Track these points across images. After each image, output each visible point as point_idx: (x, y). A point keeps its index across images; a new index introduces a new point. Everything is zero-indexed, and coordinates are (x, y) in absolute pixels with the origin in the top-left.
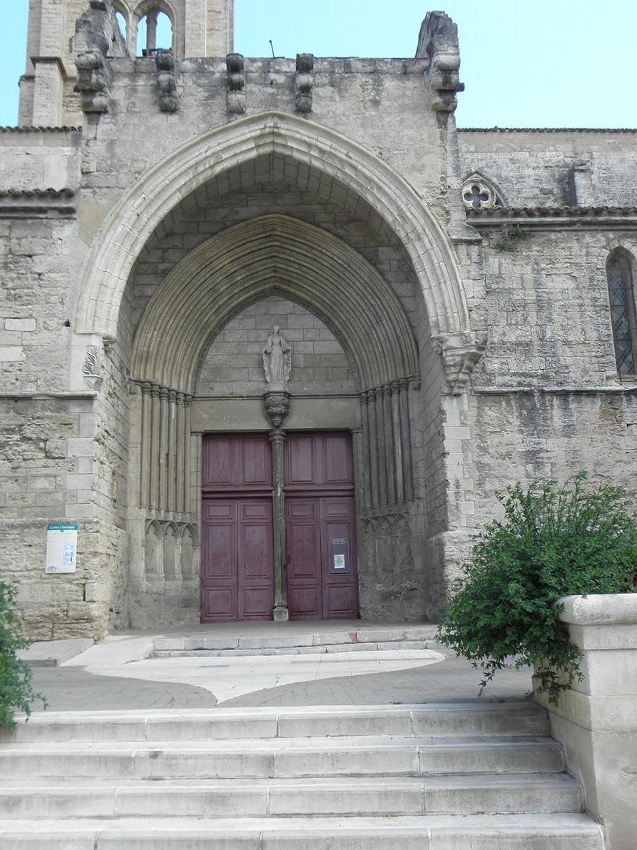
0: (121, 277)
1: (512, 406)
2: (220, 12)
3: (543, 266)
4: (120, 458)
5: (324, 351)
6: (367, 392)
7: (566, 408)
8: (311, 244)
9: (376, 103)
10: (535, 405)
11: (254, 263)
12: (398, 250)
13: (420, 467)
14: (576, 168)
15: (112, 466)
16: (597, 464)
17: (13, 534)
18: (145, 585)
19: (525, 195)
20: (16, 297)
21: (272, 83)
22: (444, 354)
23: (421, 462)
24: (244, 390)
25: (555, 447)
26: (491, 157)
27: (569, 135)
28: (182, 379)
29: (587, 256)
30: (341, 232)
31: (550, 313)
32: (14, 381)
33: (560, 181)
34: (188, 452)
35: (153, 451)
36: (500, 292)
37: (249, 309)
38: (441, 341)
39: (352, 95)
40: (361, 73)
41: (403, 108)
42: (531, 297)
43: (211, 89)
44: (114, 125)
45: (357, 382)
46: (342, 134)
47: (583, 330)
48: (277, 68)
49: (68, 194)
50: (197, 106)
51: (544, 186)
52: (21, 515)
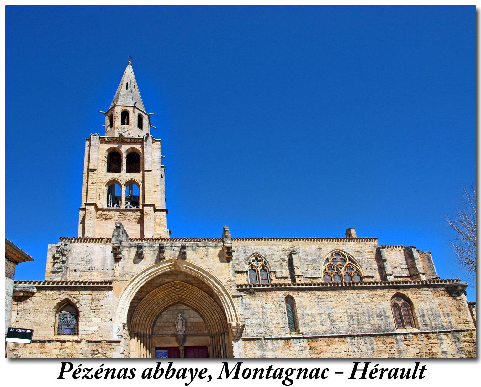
3: (264, 301)
5: (197, 321)
9: (207, 255)
10: (263, 342)
14: (292, 252)
19: (275, 261)
21: (173, 250)
29: (278, 297)
30: (200, 286)
32: (95, 336)
37: (171, 308)
38: (231, 325)
42: (260, 310)
46: (197, 264)
47: (278, 319)
48: (175, 245)
50: (150, 256)
51: (282, 257)
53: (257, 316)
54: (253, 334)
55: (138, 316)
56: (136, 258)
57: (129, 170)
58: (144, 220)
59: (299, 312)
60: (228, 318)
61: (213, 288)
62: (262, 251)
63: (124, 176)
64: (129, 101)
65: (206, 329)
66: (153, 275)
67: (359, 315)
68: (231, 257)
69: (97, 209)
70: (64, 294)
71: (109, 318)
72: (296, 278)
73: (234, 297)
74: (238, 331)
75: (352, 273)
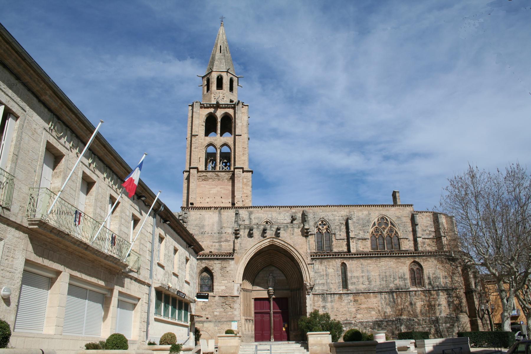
7: (331, 297)
16: (337, 308)
17: (225, 323)
18: (245, 333)
19: (335, 225)
25: (329, 305)
30: (286, 254)
36: (318, 272)
38: (306, 284)
42: (325, 274)
51: (341, 222)
52: (226, 319)
53: (322, 278)
58: (235, 182)
59: (349, 274)
60: (304, 279)
61: (296, 258)
62: (326, 216)
64: (222, 66)
66: (259, 249)
67: (387, 277)
69: (198, 171)
70: (204, 263)
72: (350, 240)
73: (309, 264)
75: (392, 235)
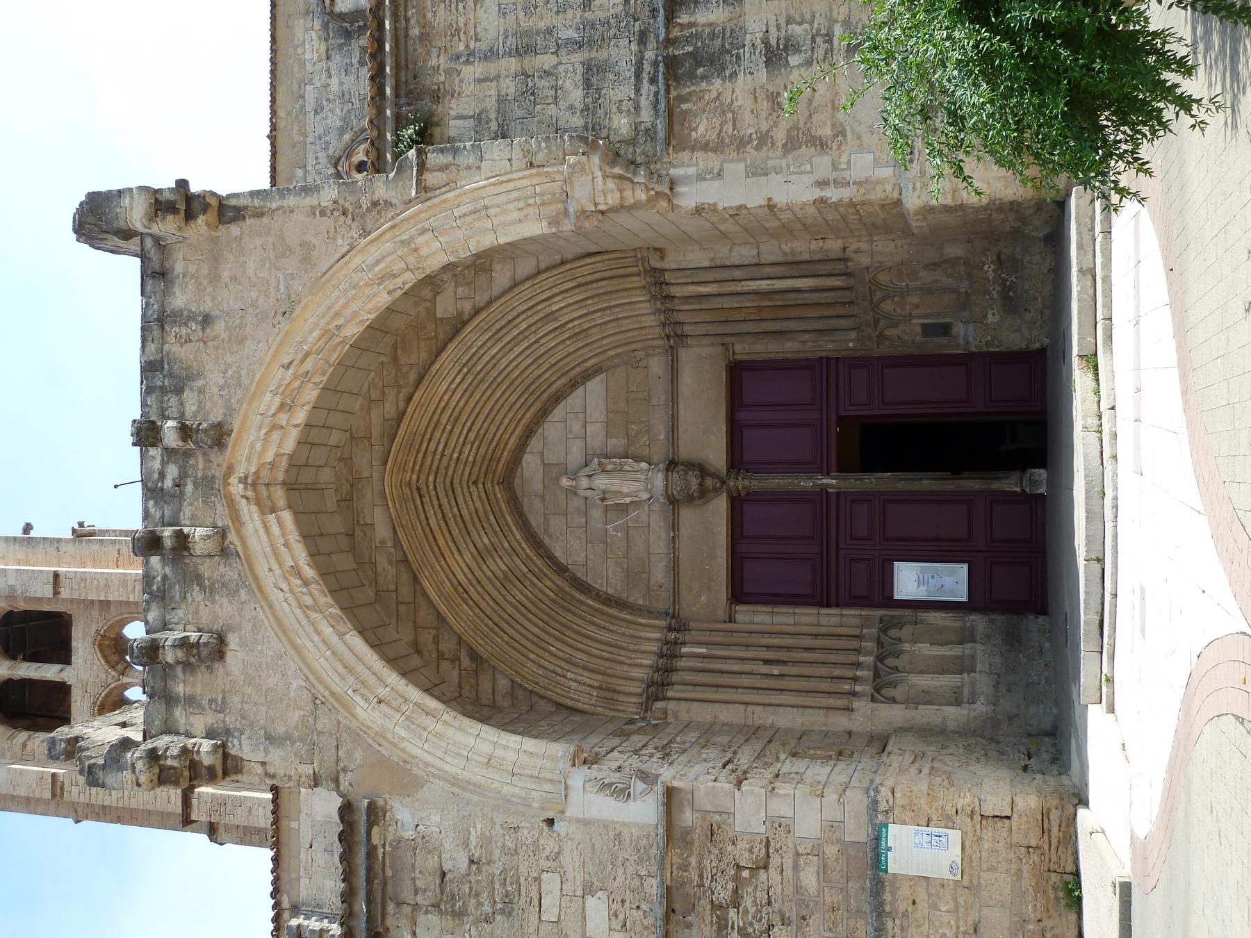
0: (476, 733)
1: (690, 93)
2: (119, 550)
3: (462, 47)
4: (770, 741)
5: (602, 406)
6: (668, 337)
8: (432, 425)
9: (207, 320)
11: (461, 516)
12: (440, 287)
13: (792, 248)
15: (783, 757)
18: (981, 708)
20: (508, 901)
22: (601, 207)
23: (784, 247)
24: (663, 535)
26: (312, 143)
27: (280, 23)
28: (641, 634)
30: (412, 377)
31: (538, 33)
32: (641, 913)
33: (347, 35)
34: (761, 628)
35: (759, 686)
36: (502, 114)
37: (534, 524)
39: (195, 358)
40: (163, 344)
41: (214, 278)
42: (512, 64)
43: (188, 579)
44: (242, 733)
45: (651, 352)
48: (156, 476)
49: (346, 811)
51: (355, 60)
54: (644, 102)
55: (565, 677)
56: (221, 671)
57: (61, 653)
63: (82, 675)
65: (642, 364)
68: (214, 202)
71: (541, 832)
74: (621, 177)
